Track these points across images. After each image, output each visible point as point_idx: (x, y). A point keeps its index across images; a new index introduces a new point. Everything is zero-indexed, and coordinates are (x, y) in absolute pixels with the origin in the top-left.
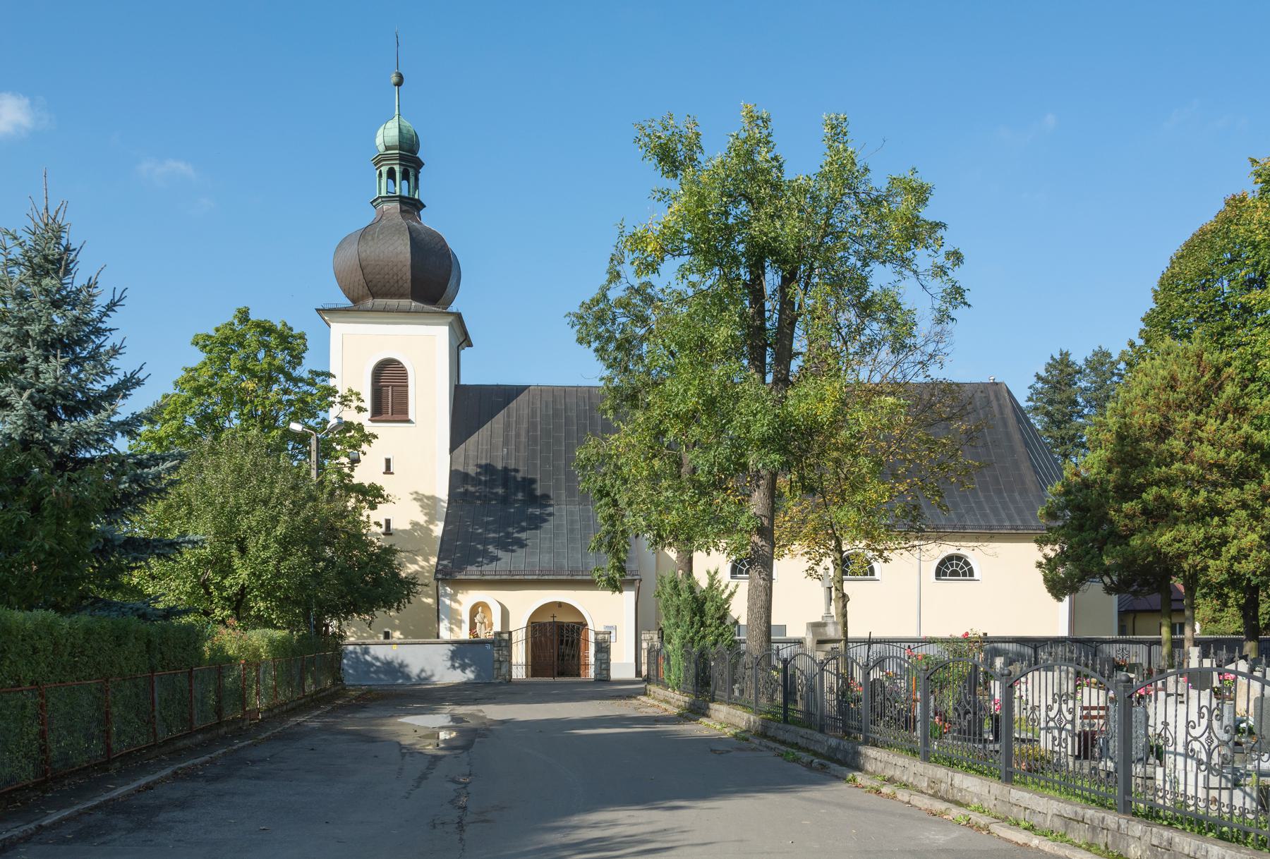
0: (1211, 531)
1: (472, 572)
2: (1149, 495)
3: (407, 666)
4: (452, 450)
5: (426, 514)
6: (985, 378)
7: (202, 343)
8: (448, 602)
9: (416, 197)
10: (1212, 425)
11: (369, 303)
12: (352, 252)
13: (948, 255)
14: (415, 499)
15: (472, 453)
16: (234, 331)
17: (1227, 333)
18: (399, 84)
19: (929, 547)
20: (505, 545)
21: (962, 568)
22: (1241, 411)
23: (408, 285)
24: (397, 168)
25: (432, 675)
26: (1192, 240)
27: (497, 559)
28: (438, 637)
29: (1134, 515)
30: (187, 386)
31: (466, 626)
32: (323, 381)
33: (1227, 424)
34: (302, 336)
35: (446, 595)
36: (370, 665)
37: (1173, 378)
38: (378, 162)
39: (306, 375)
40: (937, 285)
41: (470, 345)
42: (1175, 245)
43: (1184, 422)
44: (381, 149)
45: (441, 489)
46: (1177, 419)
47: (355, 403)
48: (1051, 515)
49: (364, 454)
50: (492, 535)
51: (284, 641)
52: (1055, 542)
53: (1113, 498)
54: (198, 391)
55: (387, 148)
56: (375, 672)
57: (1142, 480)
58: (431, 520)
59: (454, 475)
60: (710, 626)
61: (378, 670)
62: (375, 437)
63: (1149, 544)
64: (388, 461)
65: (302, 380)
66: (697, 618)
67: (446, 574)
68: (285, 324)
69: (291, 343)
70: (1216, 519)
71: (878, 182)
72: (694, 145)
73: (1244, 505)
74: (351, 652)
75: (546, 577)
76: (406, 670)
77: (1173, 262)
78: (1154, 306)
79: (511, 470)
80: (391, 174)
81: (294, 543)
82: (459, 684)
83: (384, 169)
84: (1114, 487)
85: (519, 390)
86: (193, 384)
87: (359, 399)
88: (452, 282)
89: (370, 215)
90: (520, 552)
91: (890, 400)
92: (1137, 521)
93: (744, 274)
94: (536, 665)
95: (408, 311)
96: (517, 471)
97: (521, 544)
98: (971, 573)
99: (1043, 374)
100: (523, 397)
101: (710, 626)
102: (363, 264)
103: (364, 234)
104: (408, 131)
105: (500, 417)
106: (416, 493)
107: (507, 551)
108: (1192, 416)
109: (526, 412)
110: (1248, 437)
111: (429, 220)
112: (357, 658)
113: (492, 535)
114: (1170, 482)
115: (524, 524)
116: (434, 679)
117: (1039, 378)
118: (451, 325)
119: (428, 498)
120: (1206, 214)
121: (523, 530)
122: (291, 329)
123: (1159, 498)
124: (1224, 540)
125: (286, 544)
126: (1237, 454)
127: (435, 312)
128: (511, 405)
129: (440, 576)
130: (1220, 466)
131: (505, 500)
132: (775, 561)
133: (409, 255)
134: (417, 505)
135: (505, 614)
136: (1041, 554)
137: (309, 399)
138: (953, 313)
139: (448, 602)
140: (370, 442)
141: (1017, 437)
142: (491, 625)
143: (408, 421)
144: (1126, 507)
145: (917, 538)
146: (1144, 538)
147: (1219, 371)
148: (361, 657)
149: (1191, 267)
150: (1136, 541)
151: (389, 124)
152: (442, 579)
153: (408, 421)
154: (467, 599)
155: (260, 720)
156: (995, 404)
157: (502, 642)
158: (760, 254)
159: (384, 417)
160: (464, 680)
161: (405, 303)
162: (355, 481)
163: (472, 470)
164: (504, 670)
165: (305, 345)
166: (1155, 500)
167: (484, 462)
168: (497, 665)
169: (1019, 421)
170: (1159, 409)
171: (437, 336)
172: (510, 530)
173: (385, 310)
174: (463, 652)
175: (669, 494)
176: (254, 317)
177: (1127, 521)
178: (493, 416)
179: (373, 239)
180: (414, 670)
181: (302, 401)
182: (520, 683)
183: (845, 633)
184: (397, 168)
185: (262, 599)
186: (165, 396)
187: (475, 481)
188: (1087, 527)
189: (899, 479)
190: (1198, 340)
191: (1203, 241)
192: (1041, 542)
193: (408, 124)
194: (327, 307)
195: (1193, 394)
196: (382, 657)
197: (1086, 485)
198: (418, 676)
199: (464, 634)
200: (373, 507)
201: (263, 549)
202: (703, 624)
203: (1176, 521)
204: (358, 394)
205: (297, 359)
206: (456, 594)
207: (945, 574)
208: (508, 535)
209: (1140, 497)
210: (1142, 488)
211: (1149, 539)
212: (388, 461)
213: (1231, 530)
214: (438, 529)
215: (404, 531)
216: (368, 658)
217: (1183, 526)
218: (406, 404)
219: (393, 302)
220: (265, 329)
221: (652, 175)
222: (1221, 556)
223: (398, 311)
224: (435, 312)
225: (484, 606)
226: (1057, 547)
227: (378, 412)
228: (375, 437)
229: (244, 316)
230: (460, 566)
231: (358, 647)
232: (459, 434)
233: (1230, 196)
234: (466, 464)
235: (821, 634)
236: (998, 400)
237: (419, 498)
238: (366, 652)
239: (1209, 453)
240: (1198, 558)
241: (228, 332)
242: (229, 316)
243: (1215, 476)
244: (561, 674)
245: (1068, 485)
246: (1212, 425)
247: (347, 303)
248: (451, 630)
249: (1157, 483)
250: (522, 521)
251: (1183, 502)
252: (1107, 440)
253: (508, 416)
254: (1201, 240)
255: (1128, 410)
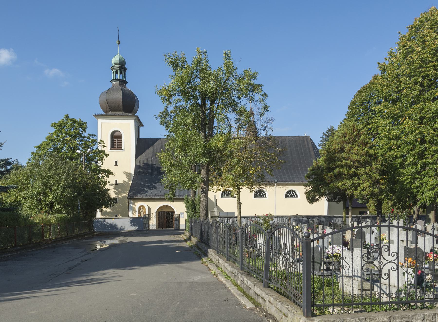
0: (355, 182)
1: (139, 196)
2: (336, 171)
3: (117, 225)
4: (136, 159)
5: (128, 179)
6: (303, 135)
7: (54, 125)
8: (132, 205)
9: (125, 80)
10: (356, 148)
11: (110, 113)
12: (104, 97)
13: (263, 95)
14: (124, 174)
15: (142, 159)
16: (64, 122)
17: (370, 119)
18: (119, 44)
19: (266, 187)
20: (150, 188)
21: (262, 194)
22: (365, 144)
23: (122, 107)
24: (118, 70)
25: (125, 228)
26: (361, 89)
27: (147, 192)
28: (129, 216)
29: (332, 177)
30: (48, 139)
31: (137, 213)
32: (93, 137)
33: (360, 148)
34: (86, 123)
35: (131, 203)
36: (105, 225)
37: (345, 133)
38: (113, 69)
39: (87, 136)
40: (260, 105)
41: (143, 126)
42: (356, 91)
43: (347, 147)
44: (113, 64)
45: (132, 171)
46: (346, 146)
47: (103, 144)
48: (308, 177)
49: (105, 160)
50: (147, 185)
51: (63, 219)
52: (309, 186)
53: (325, 171)
54: (52, 141)
55: (115, 64)
56: (107, 227)
57: (333, 166)
58: (129, 181)
59: (136, 166)
60: (198, 212)
61: (108, 227)
62: (109, 155)
63: (335, 186)
64: (116, 162)
65: (85, 137)
66: (194, 210)
67: (131, 197)
68: (80, 120)
69: (82, 125)
70: (356, 178)
71: (240, 72)
72: (184, 60)
73: (367, 174)
74: (100, 221)
75: (180, 198)
76: (117, 226)
77: (355, 97)
78: (348, 111)
79: (154, 164)
80: (117, 72)
81: (67, 187)
82: (133, 231)
83: (114, 71)
84: (326, 168)
85: (159, 139)
86: (50, 138)
87: (104, 143)
88: (136, 106)
89: (111, 85)
90: (155, 190)
91: (238, 140)
92: (332, 179)
93: (199, 102)
94: (160, 224)
95: (122, 115)
96: (155, 165)
97: (155, 188)
98: (297, 196)
99: (325, 133)
100: (158, 142)
101: (198, 212)
102: (108, 101)
103: (108, 91)
104: (122, 59)
105: (151, 148)
106: (125, 172)
107: (151, 189)
108: (350, 145)
109: (159, 147)
110: (367, 152)
111: (129, 87)
112: (102, 223)
113: (147, 185)
114: (342, 166)
115: (157, 181)
116: (125, 229)
117: (324, 134)
118: (135, 120)
119: (128, 173)
120: (366, 82)
121: (156, 183)
122: (82, 121)
123: (339, 171)
124: (359, 185)
125: (64, 188)
126: (363, 157)
127: (130, 116)
128: (155, 144)
129: (129, 198)
130: (359, 162)
131: (151, 174)
132: (209, 192)
133: (121, 98)
134: (125, 176)
135: (149, 209)
136: (306, 189)
137: (87, 143)
138: (265, 114)
139: (132, 205)
140: (107, 156)
141: (312, 153)
142: (145, 212)
143: (122, 150)
144: (329, 174)
145: (263, 185)
146: (333, 184)
147: (359, 130)
148: (103, 223)
149: (359, 98)
150: (331, 185)
151: (116, 57)
152: (130, 198)
153: (122, 150)
154: (138, 204)
155: (51, 242)
156: (305, 141)
157: (147, 218)
158: (204, 95)
159: (115, 148)
160: (134, 229)
161: (121, 113)
162: (102, 168)
163: (142, 165)
164: (147, 226)
165: (86, 126)
166: (338, 172)
167: (145, 162)
168: (144, 225)
169: (314, 148)
170: (340, 143)
171: (131, 123)
172: (152, 183)
173: (115, 115)
174: (134, 221)
175: (175, 171)
176: (70, 117)
177: (329, 179)
178: (149, 148)
179: (110, 93)
180: (119, 226)
181: (86, 143)
182: (153, 231)
183: (240, 214)
184: (118, 70)
185: (58, 205)
186: (44, 142)
187: (143, 168)
188: (318, 181)
189: (258, 166)
190: (353, 121)
191: (364, 90)
192: (305, 185)
193: (121, 56)
194: (96, 114)
195: (351, 138)
196: (109, 222)
197: (319, 167)
198: (120, 228)
199: (137, 215)
200: (108, 177)
201: (57, 189)
202: (195, 212)
203: (343, 179)
204: (103, 141)
205: (85, 130)
206: (134, 203)
207: (288, 196)
208: (151, 185)
209: (333, 171)
210: (335, 168)
211: (335, 184)
212: (116, 162)
213: (361, 181)
214: (131, 183)
215: (121, 184)
216: (105, 223)
217: (345, 180)
218: (122, 144)
219: (117, 113)
220: (74, 121)
221: (170, 71)
222: (357, 189)
223: (118, 115)
224: (130, 116)
225: (143, 207)
226: (311, 187)
227: (113, 147)
228: (109, 155)
229: (67, 117)
230: (135, 194)
231: (102, 220)
232: (138, 154)
233: (374, 75)
234: (140, 163)
235: (213, 214)
236: (307, 141)
237: (126, 173)
238: (105, 221)
239: (354, 157)
240: (351, 190)
241: (62, 122)
242: (62, 117)
243: (357, 164)
244: (167, 227)
245: (314, 168)
246: (356, 148)
247: (104, 113)
248: (133, 214)
249: (338, 167)
250: (156, 180)
251: (346, 172)
252: (324, 153)
253: (154, 148)
254: (364, 89)
255: (331, 144)
